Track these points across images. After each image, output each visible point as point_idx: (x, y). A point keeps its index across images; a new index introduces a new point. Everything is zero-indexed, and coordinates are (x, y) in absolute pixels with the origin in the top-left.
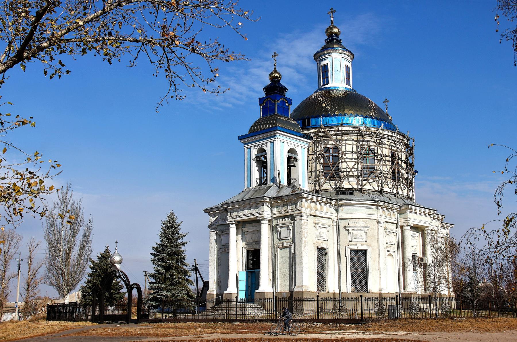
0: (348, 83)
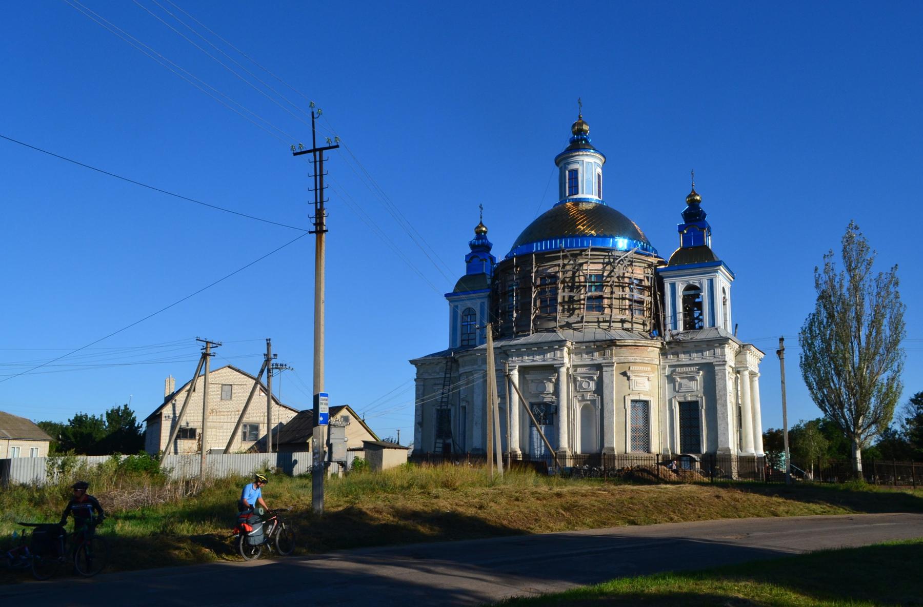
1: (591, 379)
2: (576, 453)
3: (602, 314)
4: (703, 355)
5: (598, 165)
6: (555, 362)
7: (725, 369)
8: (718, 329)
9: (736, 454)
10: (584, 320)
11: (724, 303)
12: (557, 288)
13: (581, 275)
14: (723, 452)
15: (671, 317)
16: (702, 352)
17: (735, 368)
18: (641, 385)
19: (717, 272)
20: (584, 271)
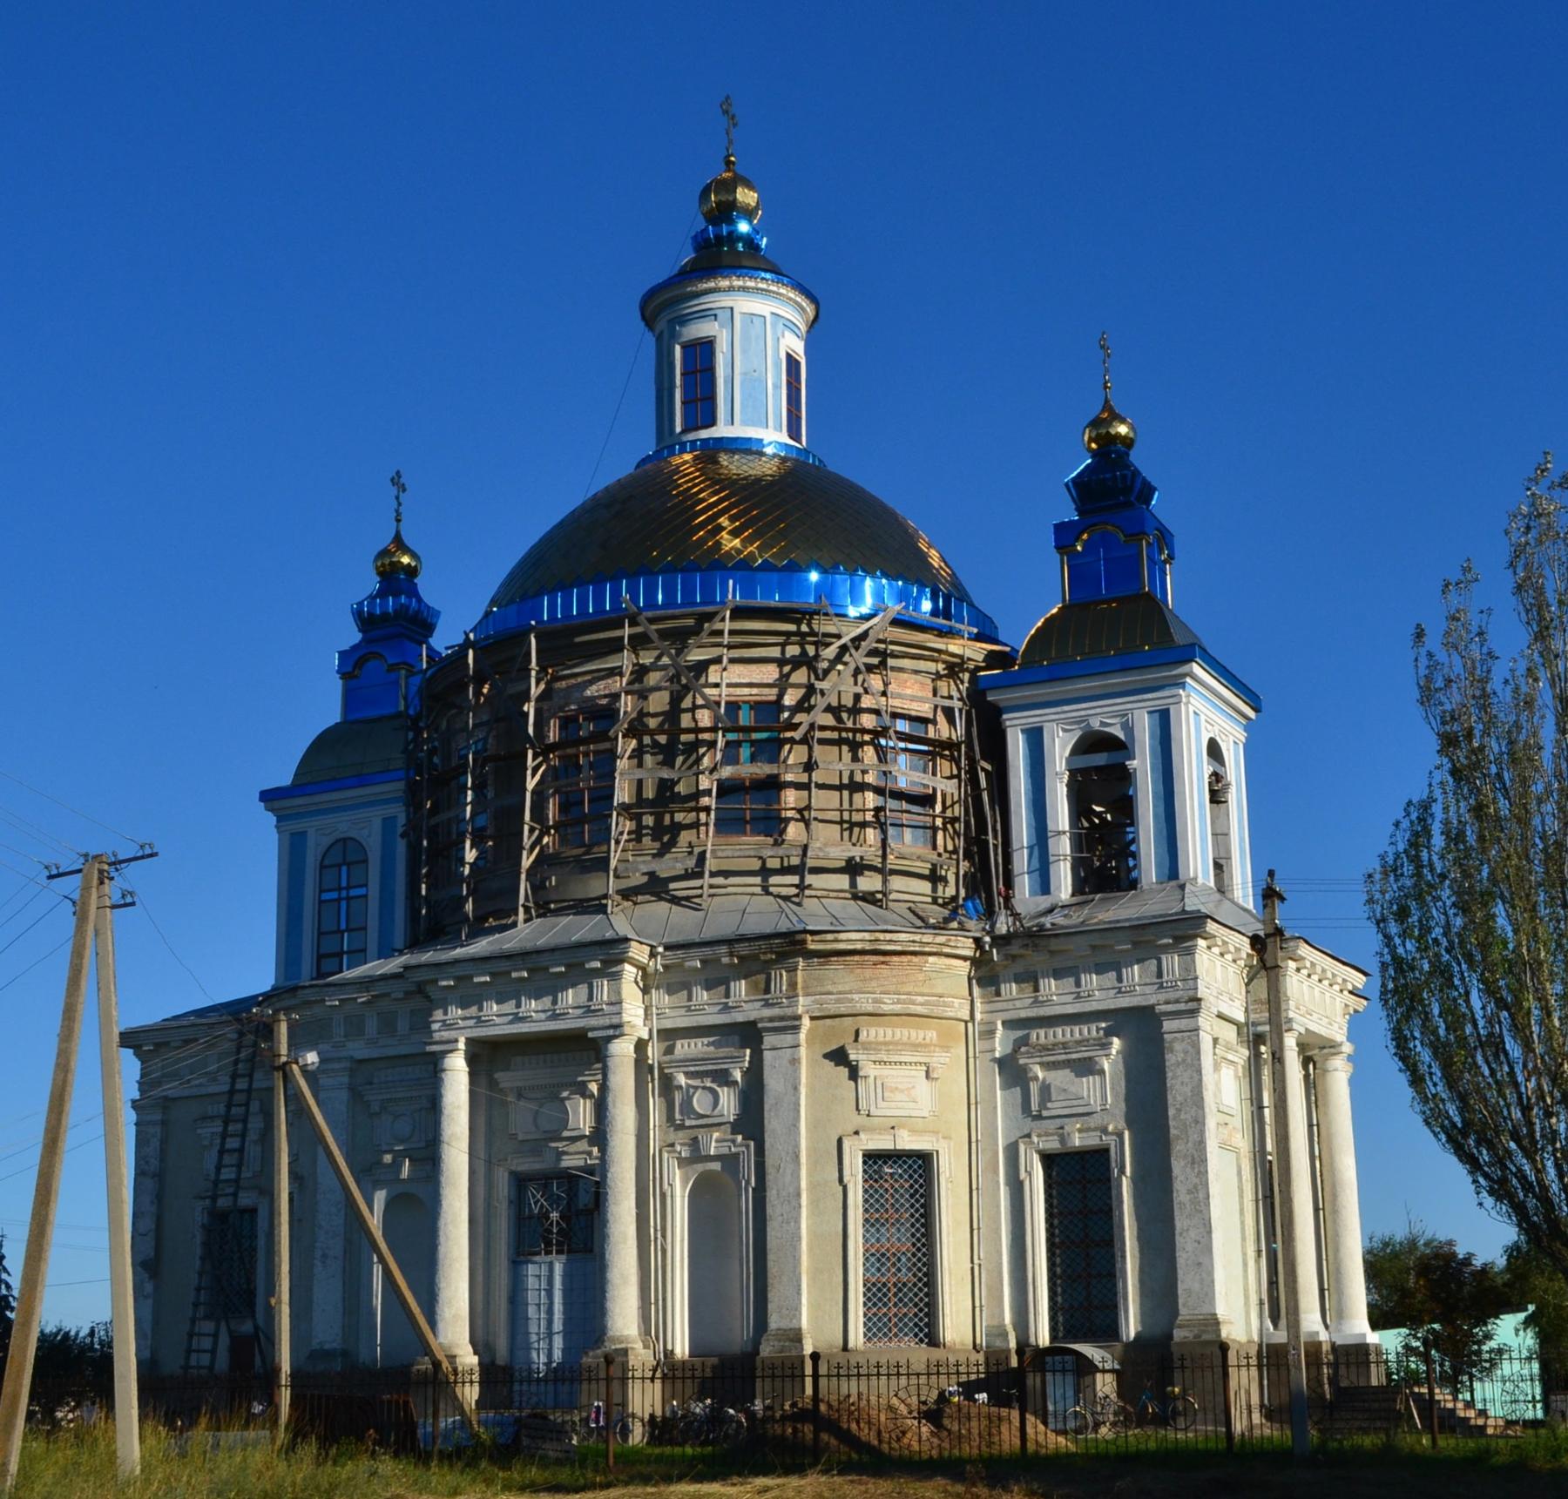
0: (794, 432)
1: (723, 1078)
2: (669, 1354)
3: (776, 844)
4: (1120, 979)
5: (790, 326)
6: (593, 1022)
7: (1197, 1029)
8: (1188, 888)
9: (1256, 1338)
10: (711, 864)
11: (1217, 797)
12: (612, 756)
13: (702, 707)
14: (1196, 1331)
15: (1031, 848)
16: (1117, 967)
17: (1247, 1024)
18: (899, 1096)
19: (1183, 685)
20: (708, 691)
